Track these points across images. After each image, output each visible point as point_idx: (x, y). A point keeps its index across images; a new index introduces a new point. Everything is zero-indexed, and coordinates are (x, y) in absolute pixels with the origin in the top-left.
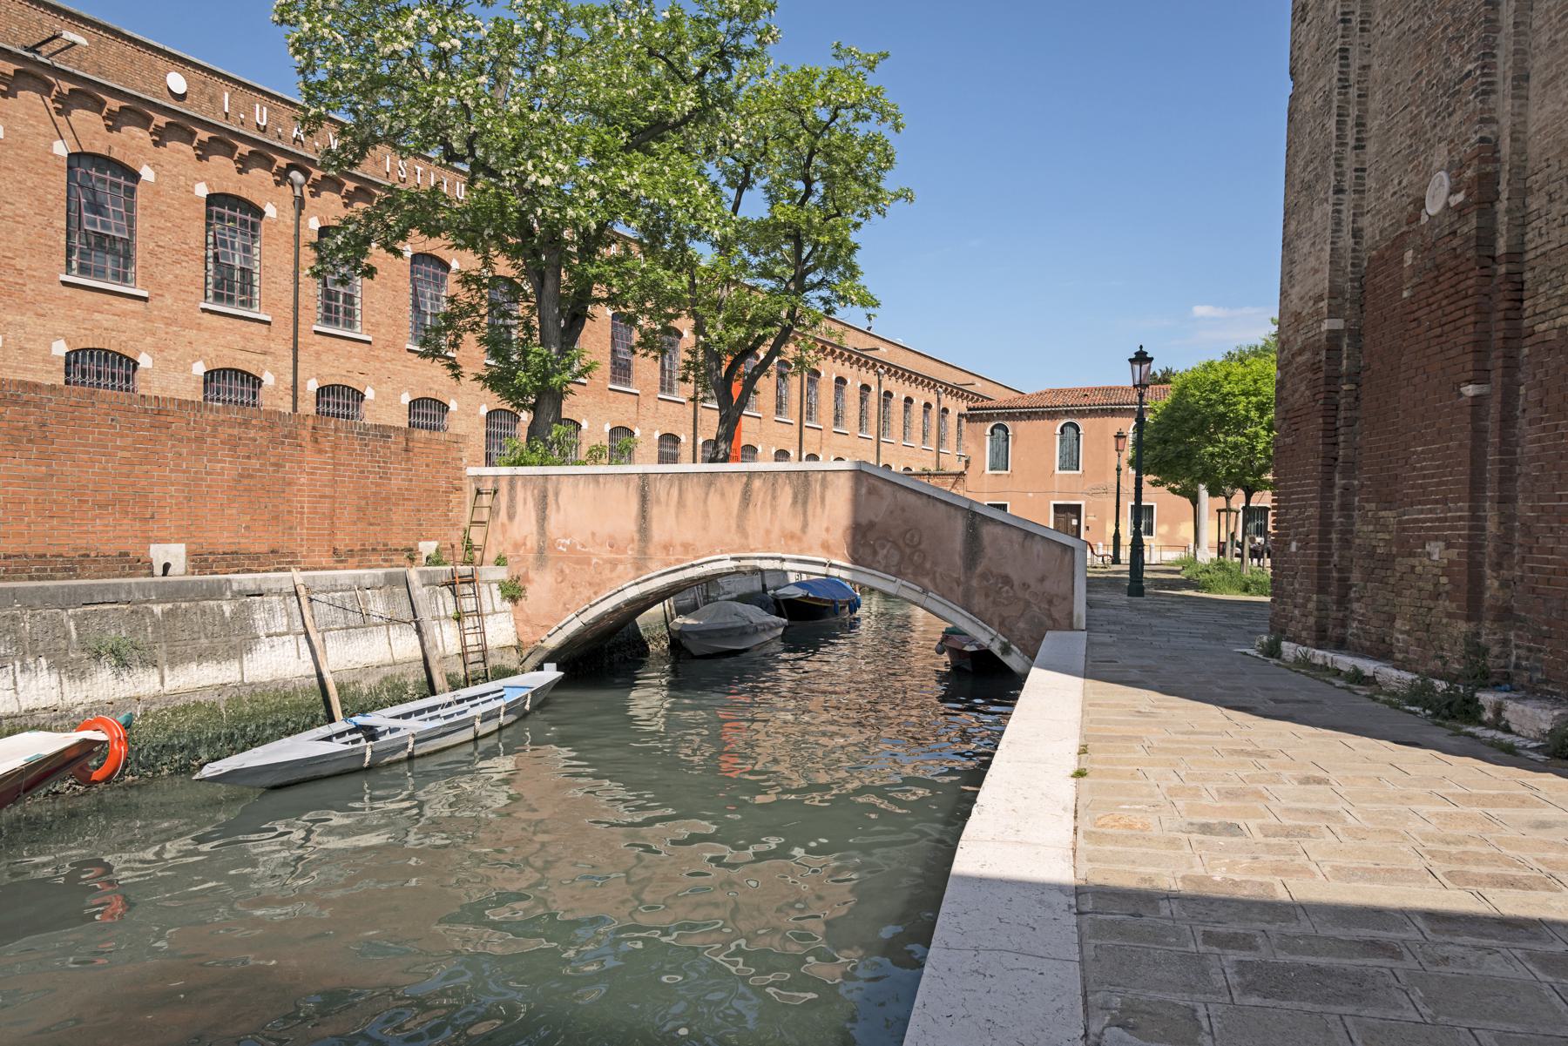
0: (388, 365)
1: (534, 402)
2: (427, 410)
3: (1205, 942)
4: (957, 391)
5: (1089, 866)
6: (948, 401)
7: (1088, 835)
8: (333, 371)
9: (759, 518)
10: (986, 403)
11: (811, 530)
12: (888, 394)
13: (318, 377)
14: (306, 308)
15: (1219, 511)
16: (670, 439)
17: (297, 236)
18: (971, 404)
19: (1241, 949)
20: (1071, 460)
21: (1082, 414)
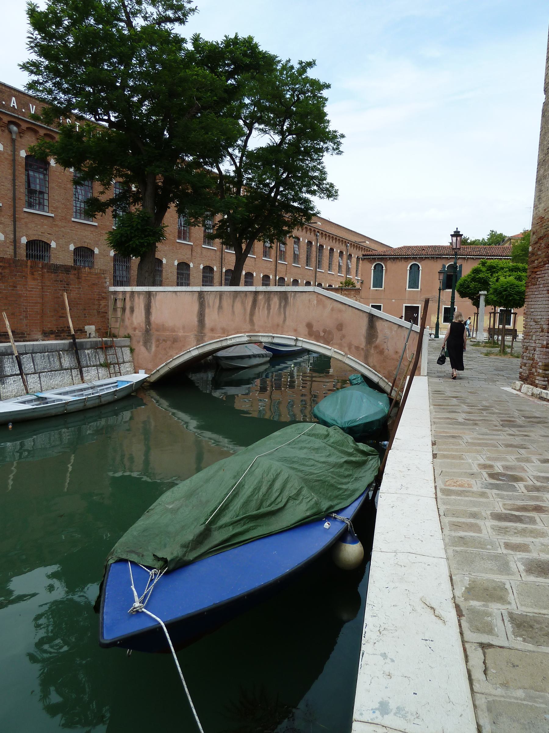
0: (63, 229)
1: (137, 246)
2: (84, 253)
3: (506, 548)
4: (357, 246)
5: (445, 507)
6: (353, 251)
7: (443, 491)
8: (35, 232)
9: (261, 314)
10: (370, 253)
11: (287, 323)
12: (321, 246)
13: (27, 236)
14: (20, 199)
15: (490, 313)
16: (208, 269)
17: (14, 160)
18: (363, 253)
19: (523, 551)
20: (414, 283)
21: (421, 259)
